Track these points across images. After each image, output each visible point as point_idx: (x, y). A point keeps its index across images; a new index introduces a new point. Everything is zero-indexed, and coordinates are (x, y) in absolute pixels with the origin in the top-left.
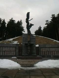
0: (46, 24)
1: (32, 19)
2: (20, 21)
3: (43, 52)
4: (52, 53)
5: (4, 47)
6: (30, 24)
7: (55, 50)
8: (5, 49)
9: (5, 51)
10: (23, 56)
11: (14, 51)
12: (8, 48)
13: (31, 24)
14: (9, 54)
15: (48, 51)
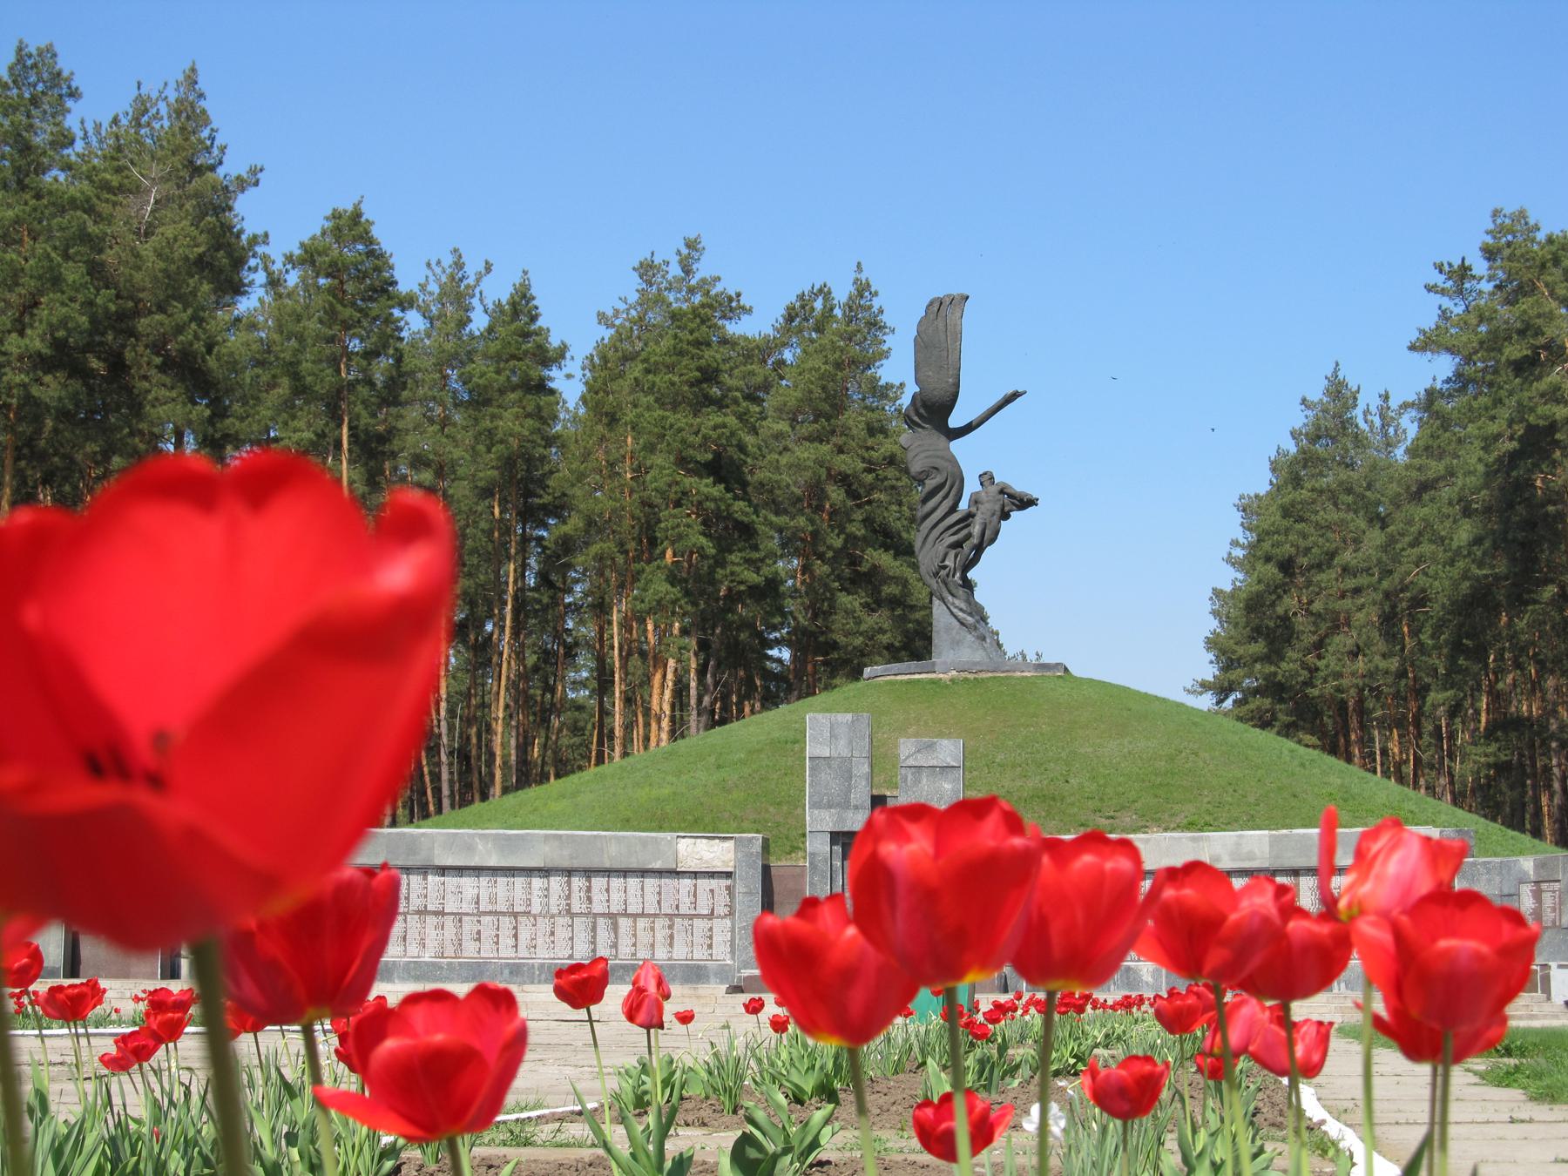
0: (1426, 343)
1: (1015, 396)
2: (842, 293)
5: (608, 872)
6: (971, 486)
8: (616, 897)
9: (612, 917)
11: (711, 916)
12: (651, 883)
13: (986, 478)
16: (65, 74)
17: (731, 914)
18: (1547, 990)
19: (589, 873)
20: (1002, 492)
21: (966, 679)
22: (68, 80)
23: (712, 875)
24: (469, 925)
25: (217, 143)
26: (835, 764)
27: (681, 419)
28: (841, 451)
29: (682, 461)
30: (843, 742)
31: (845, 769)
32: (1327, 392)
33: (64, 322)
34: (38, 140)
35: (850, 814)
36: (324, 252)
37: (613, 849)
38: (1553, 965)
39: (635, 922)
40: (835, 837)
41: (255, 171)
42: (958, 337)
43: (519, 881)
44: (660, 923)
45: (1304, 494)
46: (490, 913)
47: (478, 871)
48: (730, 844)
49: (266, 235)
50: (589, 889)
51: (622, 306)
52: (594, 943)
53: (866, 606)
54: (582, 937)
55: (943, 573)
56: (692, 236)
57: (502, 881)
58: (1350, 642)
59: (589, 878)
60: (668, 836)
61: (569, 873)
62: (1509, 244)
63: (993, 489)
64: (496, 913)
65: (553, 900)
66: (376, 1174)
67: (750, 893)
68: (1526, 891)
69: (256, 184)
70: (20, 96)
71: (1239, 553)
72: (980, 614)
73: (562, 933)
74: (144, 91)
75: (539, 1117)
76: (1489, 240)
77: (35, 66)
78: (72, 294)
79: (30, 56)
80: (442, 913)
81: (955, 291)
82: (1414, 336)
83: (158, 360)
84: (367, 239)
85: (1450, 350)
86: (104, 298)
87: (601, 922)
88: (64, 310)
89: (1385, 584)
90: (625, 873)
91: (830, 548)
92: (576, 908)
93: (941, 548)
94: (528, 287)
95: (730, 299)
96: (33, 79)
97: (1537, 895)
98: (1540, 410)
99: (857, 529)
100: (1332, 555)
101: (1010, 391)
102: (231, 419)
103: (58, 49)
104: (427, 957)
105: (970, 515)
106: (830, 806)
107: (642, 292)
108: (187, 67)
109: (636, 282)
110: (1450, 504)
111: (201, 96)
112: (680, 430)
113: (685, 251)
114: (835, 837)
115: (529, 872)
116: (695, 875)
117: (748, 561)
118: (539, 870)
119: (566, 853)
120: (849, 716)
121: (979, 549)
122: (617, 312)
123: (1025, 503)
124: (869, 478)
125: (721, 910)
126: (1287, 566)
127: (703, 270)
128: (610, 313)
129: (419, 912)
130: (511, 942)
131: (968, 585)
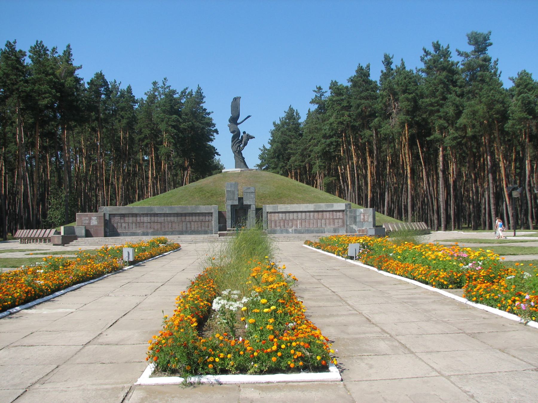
0: (312, 102)
1: (249, 117)
6: (242, 134)
35: (234, 201)
39: (191, 223)
51: (149, 91)
75: (319, 248)
81: (238, 96)
87: (188, 223)
93: (237, 146)
97: (364, 216)
106: (231, 200)
107: (154, 88)
109: (152, 86)
113: (164, 80)
123: (252, 137)
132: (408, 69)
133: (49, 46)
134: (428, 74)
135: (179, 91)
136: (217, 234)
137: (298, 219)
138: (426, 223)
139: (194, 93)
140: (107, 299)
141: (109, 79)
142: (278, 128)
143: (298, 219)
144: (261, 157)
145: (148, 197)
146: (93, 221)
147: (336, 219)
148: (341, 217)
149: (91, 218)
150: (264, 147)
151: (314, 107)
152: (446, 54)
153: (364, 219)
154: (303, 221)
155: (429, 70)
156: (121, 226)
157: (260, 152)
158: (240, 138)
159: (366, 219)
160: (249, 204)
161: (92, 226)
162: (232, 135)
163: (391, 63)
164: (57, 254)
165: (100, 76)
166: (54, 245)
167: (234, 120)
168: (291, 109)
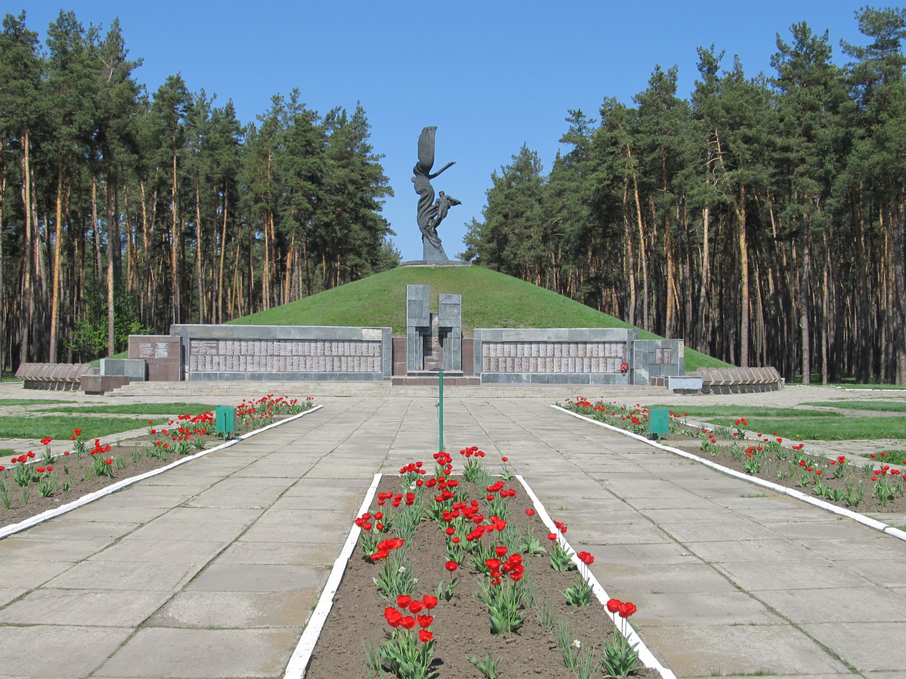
0: (566, 139)
1: (452, 164)
3: (492, 360)
4: (524, 365)
5: (338, 341)
6: (437, 197)
7: (538, 351)
8: (340, 349)
9: (339, 357)
10: (410, 374)
12: (352, 344)
13: (442, 194)
14: (356, 370)
15: (510, 357)
16: (78, 23)
17: (381, 355)
18: (667, 385)
19: (331, 341)
20: (448, 199)
21: (440, 268)
22: (80, 25)
23: (374, 342)
24: (289, 360)
25: (124, 48)
26: (417, 303)
27: (298, 159)
28: (352, 171)
29: (299, 174)
30: (420, 295)
31: (421, 304)
32: (522, 153)
33: (85, 122)
34: (70, 49)
35: (422, 320)
36: (167, 92)
37: (340, 333)
38: (669, 377)
40: (417, 328)
41: (141, 60)
42: (433, 142)
43: (307, 344)
44: (356, 359)
45: (513, 190)
46: (296, 356)
47: (292, 340)
48: (381, 331)
49: (145, 85)
50: (331, 347)
51: (266, 113)
52: (333, 366)
53: (361, 229)
54: (329, 364)
55: (428, 228)
56: (296, 88)
57: (300, 344)
58: (529, 245)
59: (331, 343)
60: (359, 328)
61: (324, 341)
62: (610, 110)
63: (445, 198)
64: (298, 356)
65: (319, 351)
66: (902, 562)
67: (387, 348)
68: (658, 351)
69: (141, 65)
70: (62, 32)
71: (485, 209)
72: (439, 241)
73: (322, 363)
74: (93, 26)
76: (602, 108)
77: (67, 20)
78: (87, 111)
79: (65, 15)
80: (279, 356)
81: (432, 125)
82: (561, 137)
83: (118, 137)
84: (183, 88)
85: (574, 142)
86: (99, 113)
87: (335, 358)
88: (85, 118)
89: (545, 225)
90: (344, 341)
91: (349, 208)
92: (326, 354)
93: (427, 218)
94: (232, 105)
95: (313, 113)
96: (66, 25)
97: (662, 353)
98: (620, 170)
99: (357, 200)
100: (522, 213)
101: (450, 162)
102: (145, 160)
103: (75, 12)
104: (274, 372)
105: (437, 207)
107: (275, 108)
108: (115, 18)
110: (578, 200)
111: (120, 30)
112: (299, 164)
113: (293, 94)
114: (417, 328)
115: (310, 341)
116: (368, 342)
117: (324, 213)
118: (314, 340)
119: (323, 334)
120: (422, 286)
121: (440, 220)
122: (264, 115)
123: (456, 203)
124: (362, 182)
125: (377, 354)
126: (506, 216)
127: (300, 101)
128: (262, 115)
129: (271, 355)
130: (304, 366)
131: (436, 232)
132: (747, 77)
133: (84, 20)
134: (783, 88)
135: (323, 114)
136: (389, 379)
137: (585, 356)
138: (779, 369)
139: (349, 119)
140: (185, 513)
141: (192, 87)
142: (500, 186)
143: (539, 356)
144: (469, 241)
145: (249, 313)
146: (159, 351)
147: (610, 357)
148: (620, 354)
149: (156, 345)
150: (474, 221)
151: (568, 149)
152: (820, 52)
153: (662, 359)
154: (548, 360)
155: (785, 80)
156: (212, 360)
157: (466, 231)
158: (434, 203)
159: (666, 360)
160: (449, 326)
161: (156, 359)
162: (419, 197)
163: (716, 68)
164: (95, 412)
165: (176, 83)
166: (87, 393)
167: (423, 170)
168: (525, 152)
